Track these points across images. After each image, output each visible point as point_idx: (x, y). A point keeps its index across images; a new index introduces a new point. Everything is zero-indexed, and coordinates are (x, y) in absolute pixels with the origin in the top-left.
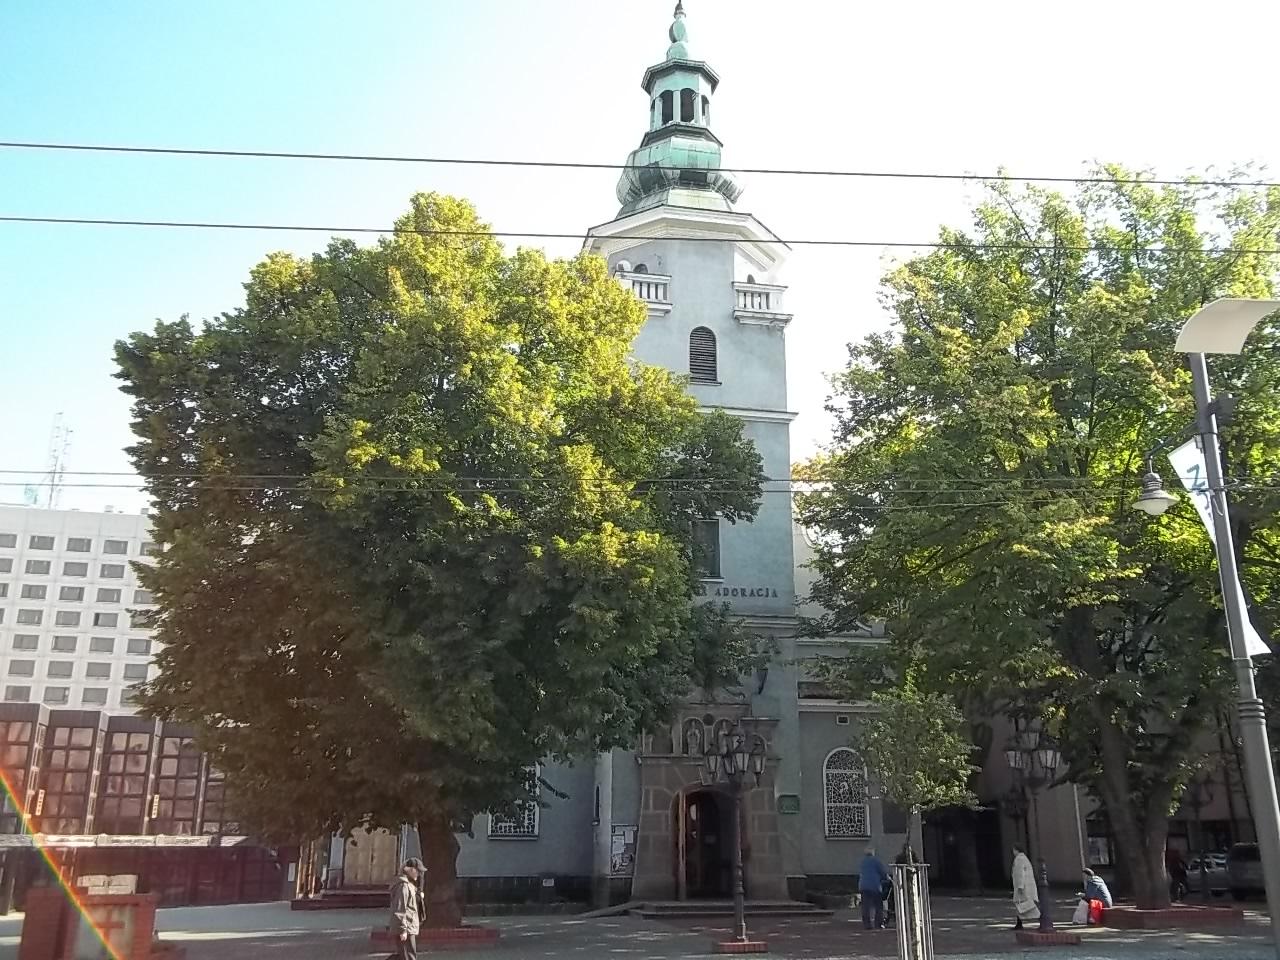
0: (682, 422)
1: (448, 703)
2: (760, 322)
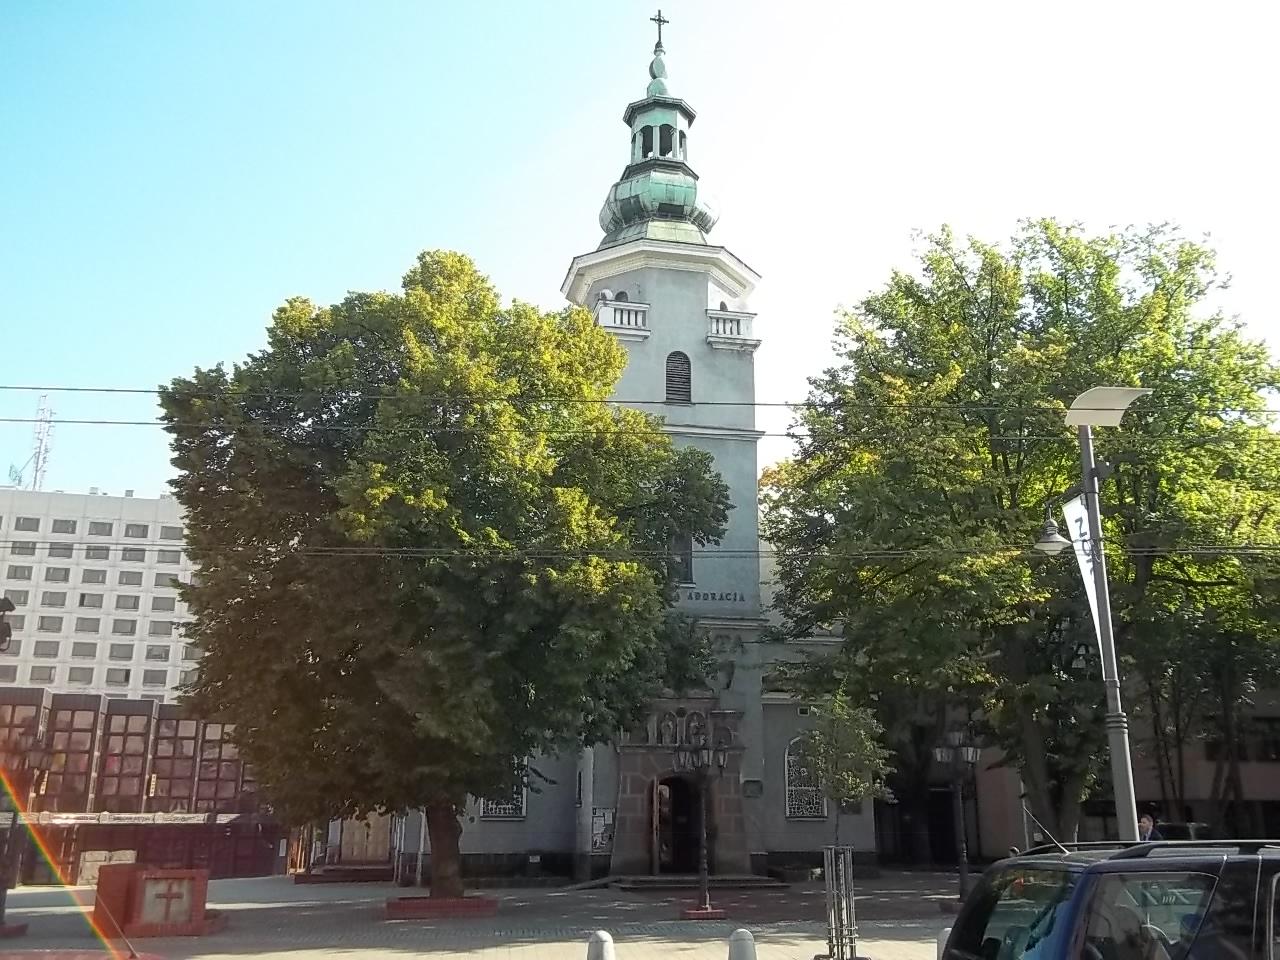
0: (658, 461)
1: (454, 707)
2: (732, 347)
